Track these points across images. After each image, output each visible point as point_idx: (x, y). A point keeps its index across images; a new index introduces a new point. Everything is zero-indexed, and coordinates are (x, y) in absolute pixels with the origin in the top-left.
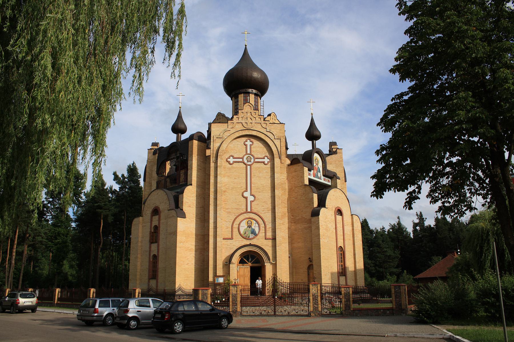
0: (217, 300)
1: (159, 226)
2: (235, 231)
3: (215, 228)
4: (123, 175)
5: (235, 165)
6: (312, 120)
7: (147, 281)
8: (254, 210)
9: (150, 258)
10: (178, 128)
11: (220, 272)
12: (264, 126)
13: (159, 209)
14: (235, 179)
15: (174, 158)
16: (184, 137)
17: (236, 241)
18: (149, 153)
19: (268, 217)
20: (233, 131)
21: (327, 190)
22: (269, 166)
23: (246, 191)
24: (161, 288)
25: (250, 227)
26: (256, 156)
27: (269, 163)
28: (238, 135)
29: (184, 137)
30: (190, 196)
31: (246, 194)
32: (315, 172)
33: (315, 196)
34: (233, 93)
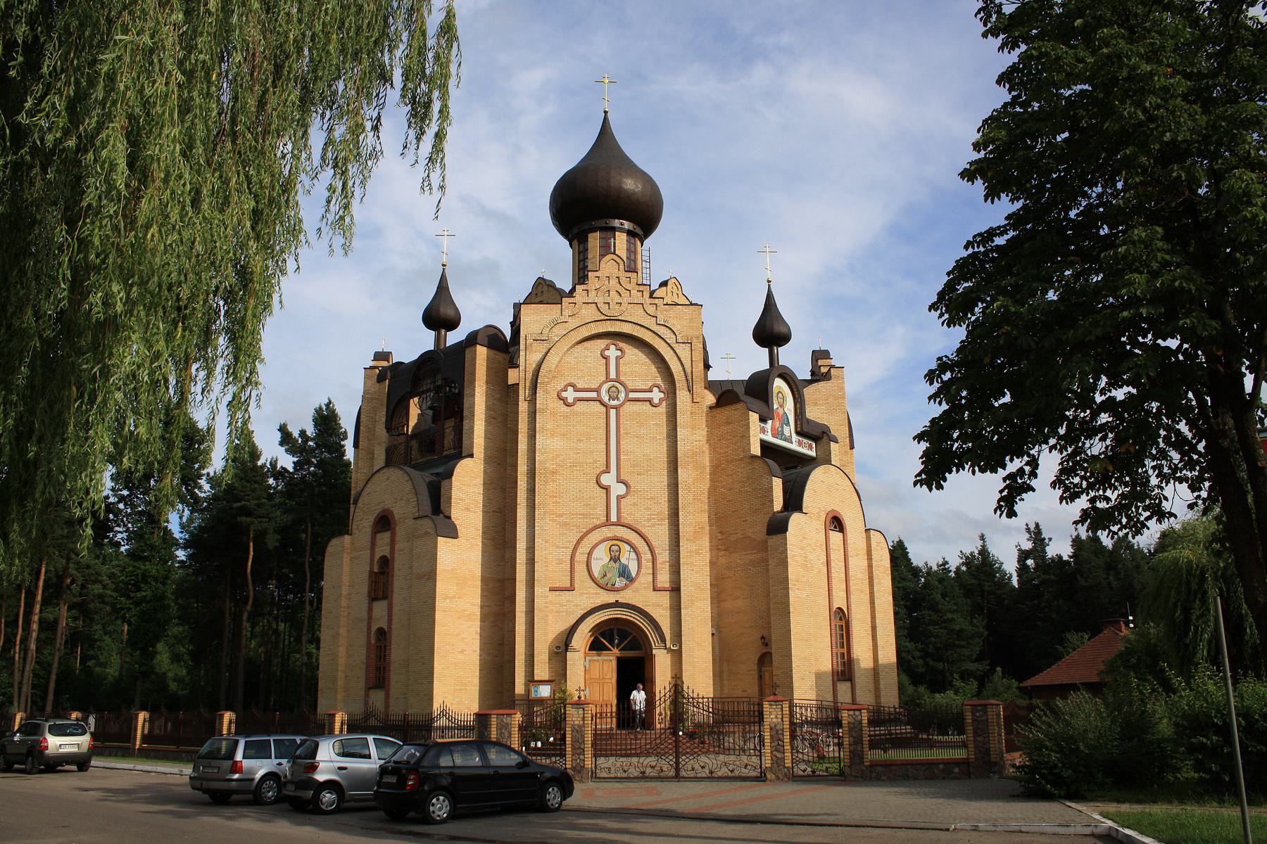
0: (536, 741)
1: (393, 557)
2: (580, 569)
3: (531, 562)
4: (303, 433)
5: (580, 407)
6: (770, 296)
7: (362, 693)
8: (627, 519)
9: (369, 637)
10: (439, 316)
11: (542, 672)
12: (651, 310)
13: (393, 516)
14: (580, 441)
15: (428, 390)
16: (453, 338)
17: (582, 594)
18: (367, 377)
19: (660, 535)
20: (574, 323)
21: (806, 469)
22: (663, 409)
23: (607, 471)
24: (396, 710)
25: (615, 559)
26: (631, 386)
27: (664, 403)
28: (587, 334)
29: (453, 338)
30: (468, 485)
31: (607, 479)
32: (777, 424)
33: (777, 484)
34: (575, 231)
